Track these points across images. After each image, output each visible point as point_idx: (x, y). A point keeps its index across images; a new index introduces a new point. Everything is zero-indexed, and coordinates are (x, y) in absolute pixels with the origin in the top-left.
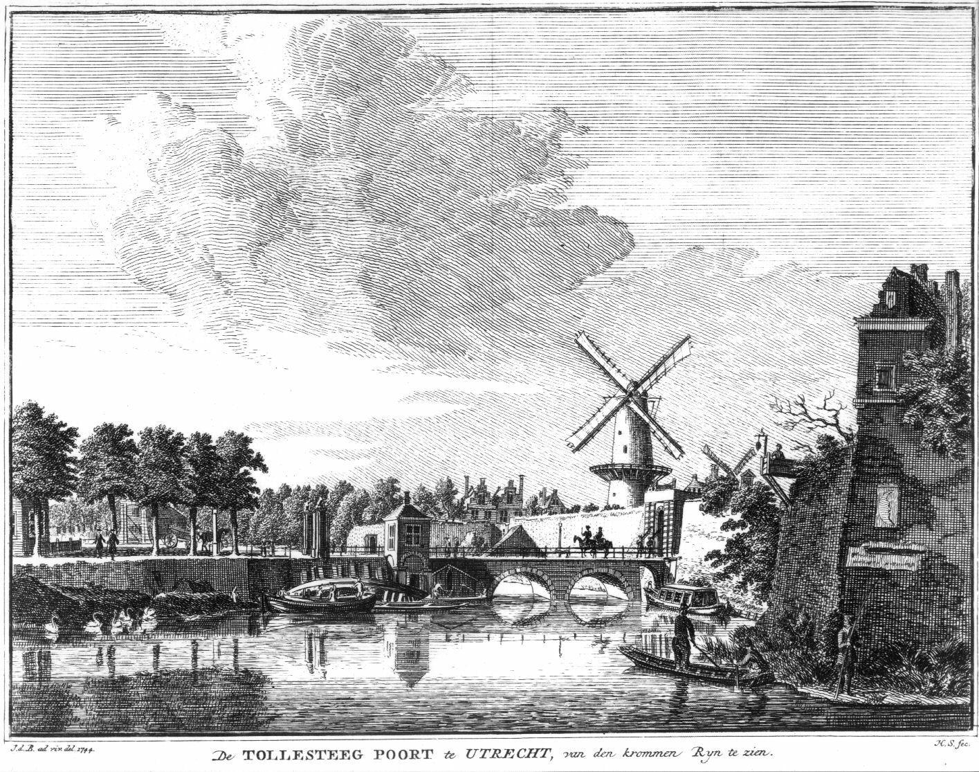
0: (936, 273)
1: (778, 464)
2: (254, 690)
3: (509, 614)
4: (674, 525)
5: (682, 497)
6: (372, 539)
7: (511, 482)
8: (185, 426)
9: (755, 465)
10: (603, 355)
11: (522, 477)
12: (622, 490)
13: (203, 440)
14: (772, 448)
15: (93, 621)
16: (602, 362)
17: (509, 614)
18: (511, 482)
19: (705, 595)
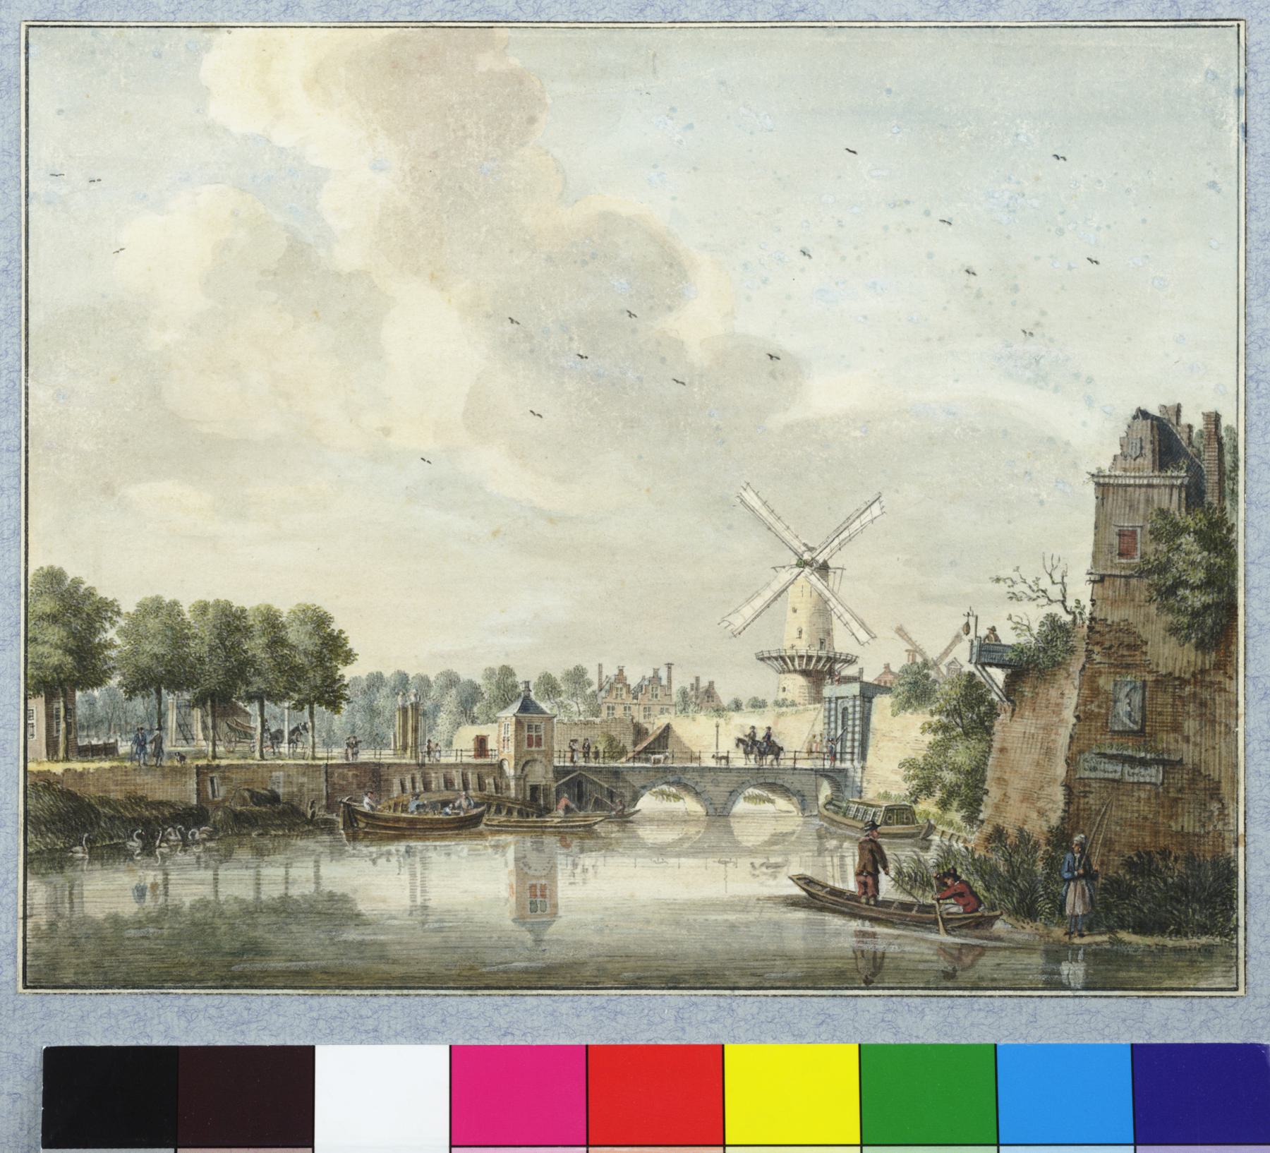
0: (1193, 418)
1: (988, 651)
2: (111, 838)
3: (648, 834)
4: (862, 719)
5: (868, 693)
6: (481, 742)
7: (656, 671)
8: (247, 598)
9: (963, 655)
10: (769, 529)
11: (669, 666)
12: (796, 685)
13: (271, 621)
14: (983, 632)
15: (133, 840)
16: (771, 519)
17: (648, 834)
18: (656, 671)
19: (900, 813)
